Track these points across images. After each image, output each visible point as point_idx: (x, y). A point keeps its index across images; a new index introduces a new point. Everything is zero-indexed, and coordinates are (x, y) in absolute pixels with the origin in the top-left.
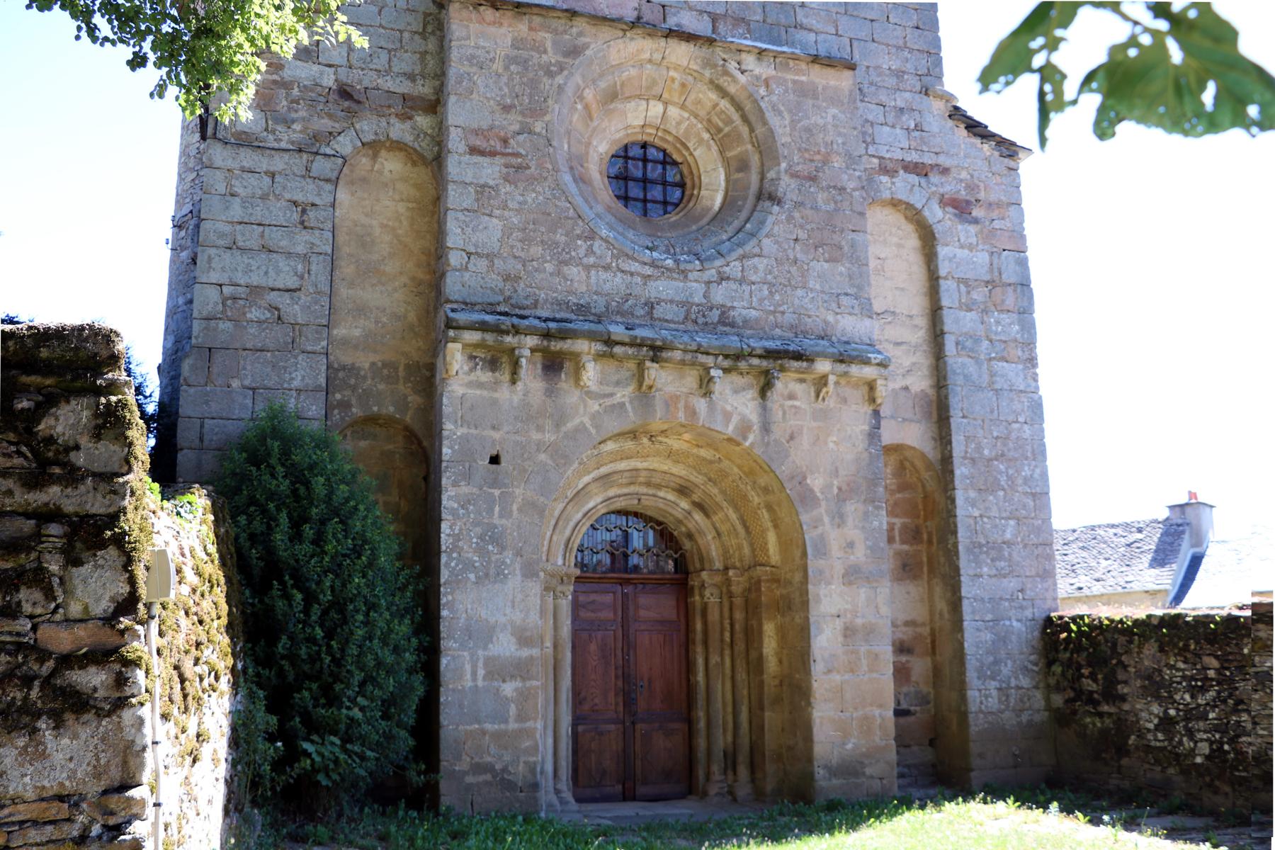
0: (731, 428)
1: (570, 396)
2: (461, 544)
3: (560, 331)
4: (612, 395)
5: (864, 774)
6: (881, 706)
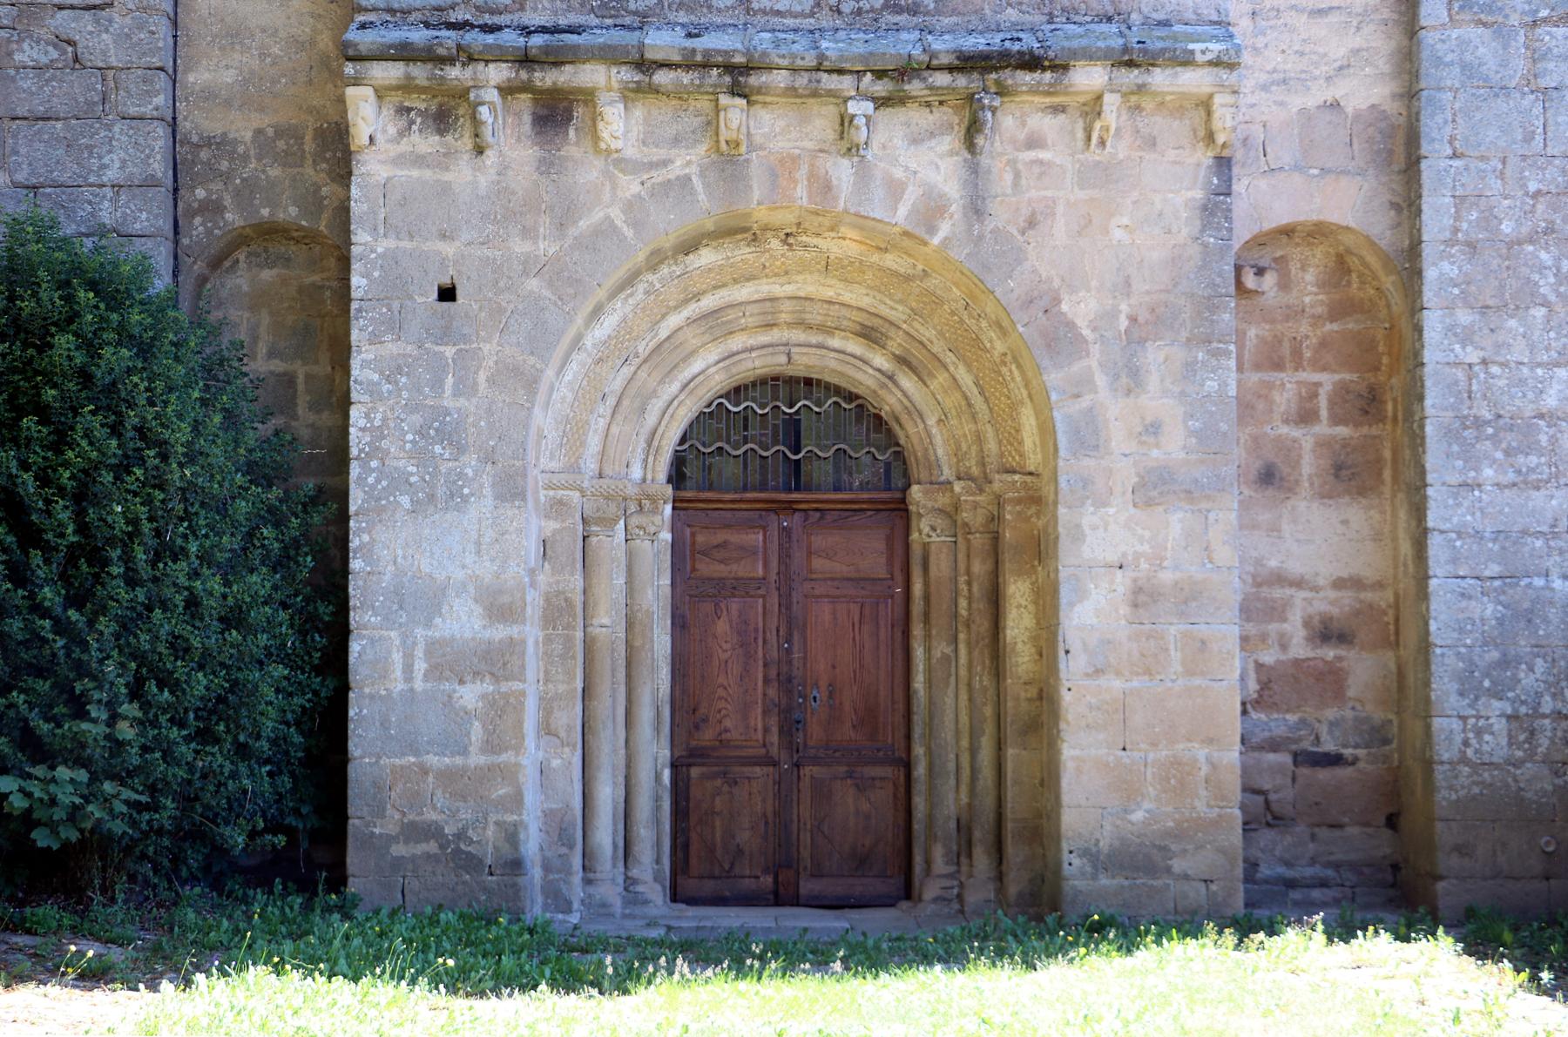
0: (902, 211)
1: (586, 171)
2: (384, 444)
3: (547, 50)
4: (665, 163)
5: (1168, 870)
6: (1210, 741)
